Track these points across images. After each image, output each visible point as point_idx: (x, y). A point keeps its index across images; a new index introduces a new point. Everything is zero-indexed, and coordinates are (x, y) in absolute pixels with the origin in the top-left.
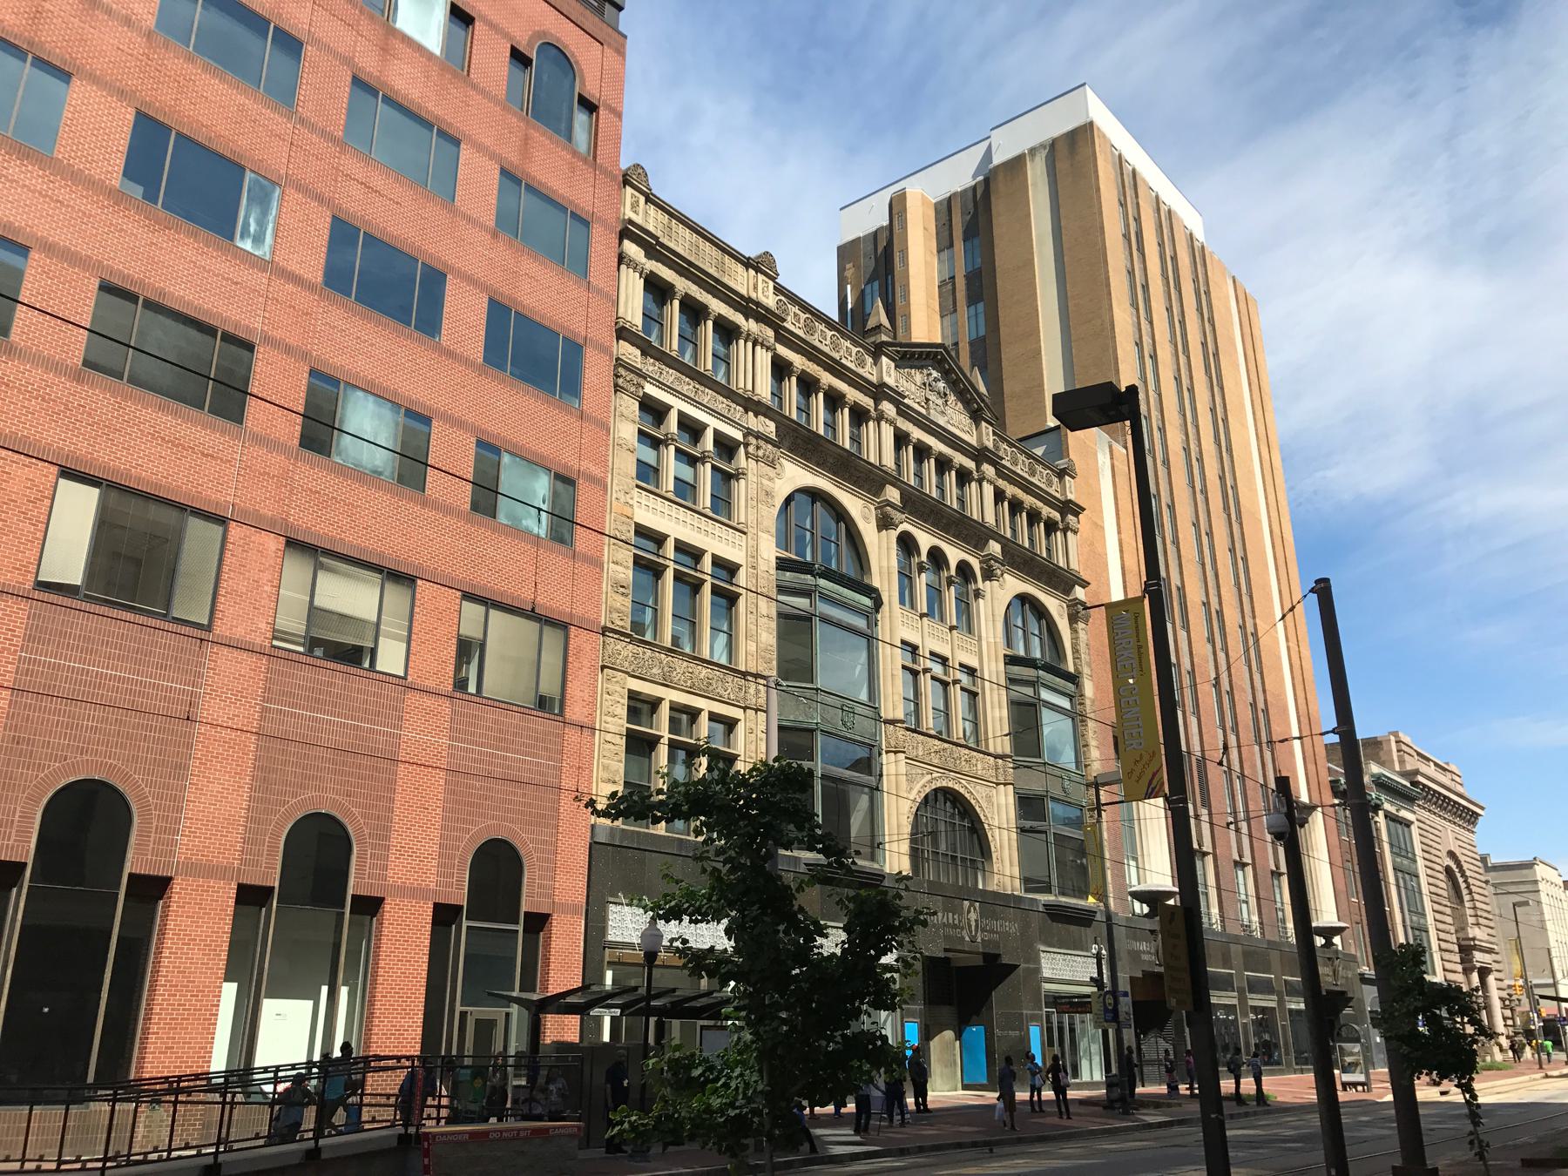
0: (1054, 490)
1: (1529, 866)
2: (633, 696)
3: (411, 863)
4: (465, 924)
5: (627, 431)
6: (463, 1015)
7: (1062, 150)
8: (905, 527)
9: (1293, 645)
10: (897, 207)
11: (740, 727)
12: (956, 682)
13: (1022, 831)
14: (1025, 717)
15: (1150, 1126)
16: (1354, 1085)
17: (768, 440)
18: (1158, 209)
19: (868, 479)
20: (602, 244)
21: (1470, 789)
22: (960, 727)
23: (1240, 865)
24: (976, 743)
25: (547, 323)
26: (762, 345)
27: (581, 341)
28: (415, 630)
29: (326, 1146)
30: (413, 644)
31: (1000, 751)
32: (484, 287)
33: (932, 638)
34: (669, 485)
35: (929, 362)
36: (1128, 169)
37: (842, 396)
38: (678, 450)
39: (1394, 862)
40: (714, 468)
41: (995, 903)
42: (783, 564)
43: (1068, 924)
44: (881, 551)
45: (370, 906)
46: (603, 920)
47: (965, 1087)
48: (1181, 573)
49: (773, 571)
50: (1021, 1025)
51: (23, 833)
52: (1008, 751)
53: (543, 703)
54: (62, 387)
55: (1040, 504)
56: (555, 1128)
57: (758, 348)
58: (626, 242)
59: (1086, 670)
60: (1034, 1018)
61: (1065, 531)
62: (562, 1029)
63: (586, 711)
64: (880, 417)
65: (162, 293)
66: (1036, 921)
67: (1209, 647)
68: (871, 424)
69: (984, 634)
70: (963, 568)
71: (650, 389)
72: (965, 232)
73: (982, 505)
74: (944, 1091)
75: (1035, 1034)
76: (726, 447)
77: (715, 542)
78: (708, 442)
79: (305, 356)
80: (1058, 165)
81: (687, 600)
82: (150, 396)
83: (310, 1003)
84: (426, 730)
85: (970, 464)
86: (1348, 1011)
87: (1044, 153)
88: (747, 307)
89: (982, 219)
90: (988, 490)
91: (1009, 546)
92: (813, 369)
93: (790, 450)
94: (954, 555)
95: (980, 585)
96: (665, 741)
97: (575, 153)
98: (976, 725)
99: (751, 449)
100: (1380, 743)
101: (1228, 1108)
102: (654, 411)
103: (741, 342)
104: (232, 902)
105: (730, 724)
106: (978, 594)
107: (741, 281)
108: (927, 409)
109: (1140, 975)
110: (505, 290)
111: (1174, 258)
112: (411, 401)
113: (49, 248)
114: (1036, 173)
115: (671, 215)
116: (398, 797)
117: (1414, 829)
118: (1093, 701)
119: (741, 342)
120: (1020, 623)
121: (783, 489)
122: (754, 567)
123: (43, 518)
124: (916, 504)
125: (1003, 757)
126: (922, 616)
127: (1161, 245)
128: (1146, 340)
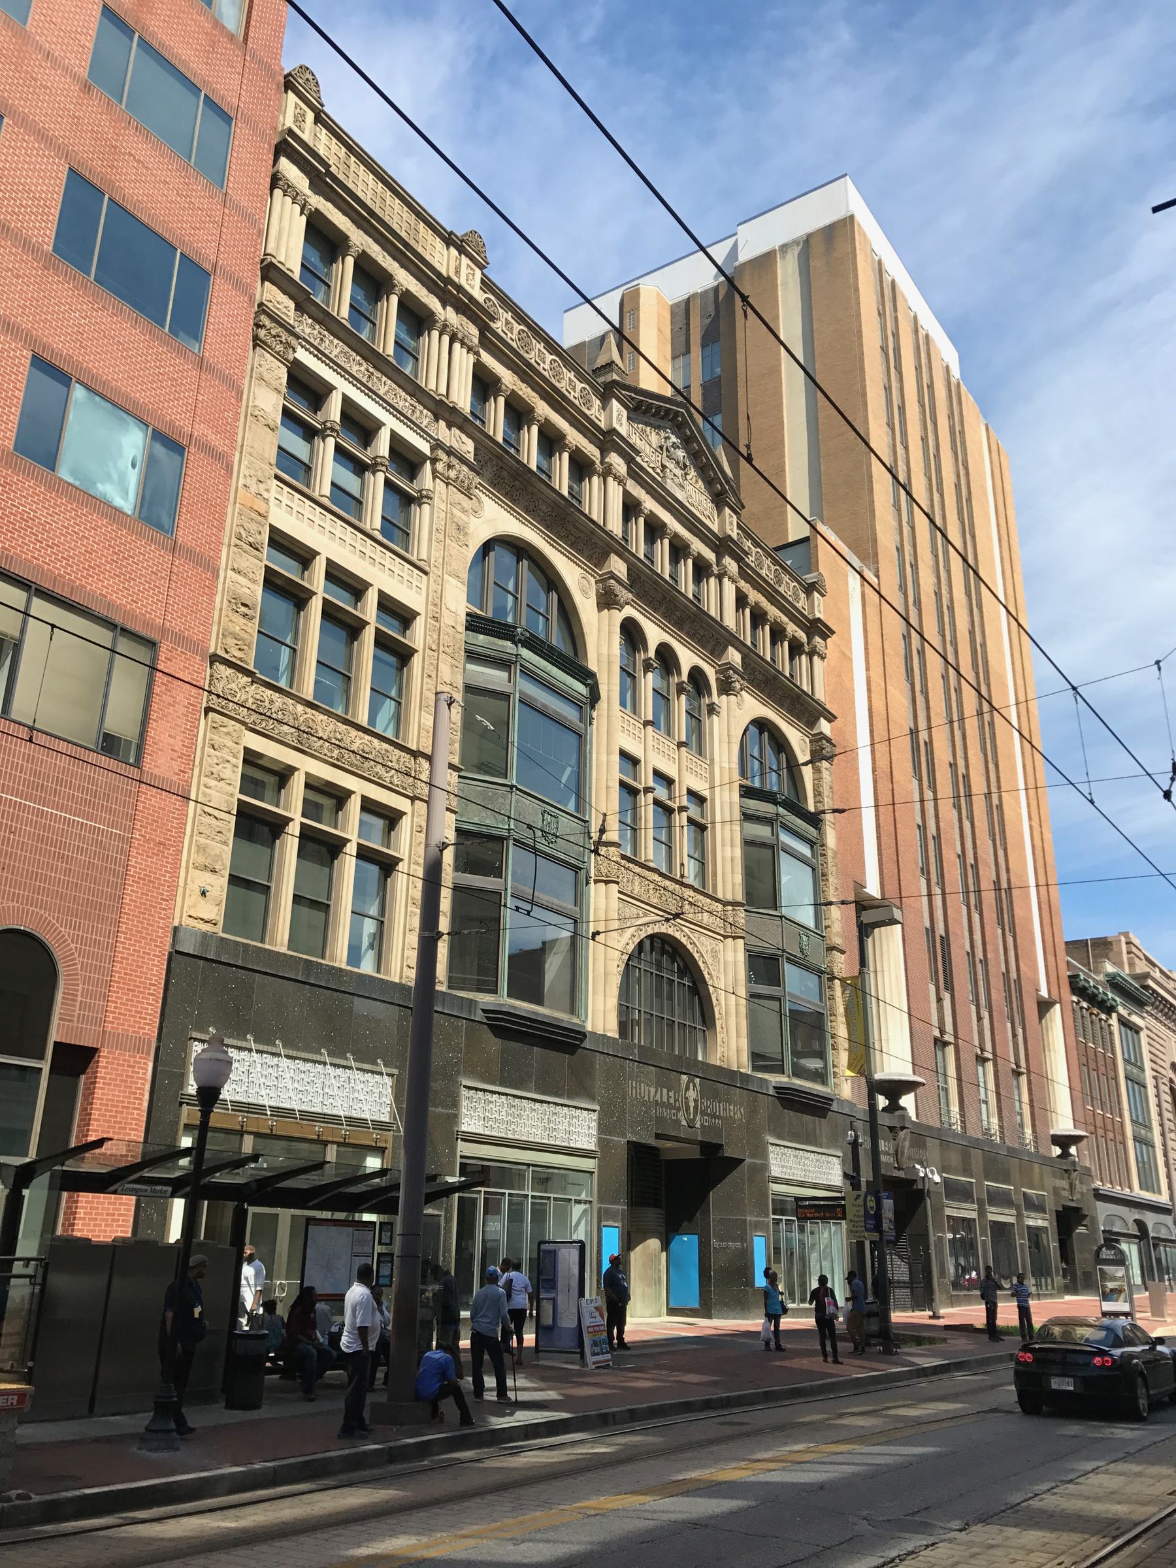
0: (802, 603)
2: (251, 758)
7: (818, 247)
8: (629, 611)
9: (1035, 824)
10: (629, 305)
11: (405, 824)
13: (752, 996)
15: (923, 1372)
17: (463, 460)
18: (916, 331)
20: (248, 157)
23: (982, 1060)
26: (463, 344)
29: (362, 1322)
31: (729, 898)
32: (63, 152)
34: (323, 488)
36: (887, 279)
37: (562, 436)
38: (339, 449)
39: (1125, 1069)
40: (388, 484)
41: (719, 1081)
42: (474, 624)
43: (805, 1110)
47: (672, 1312)
50: (742, 1233)
52: (740, 897)
53: (110, 744)
55: (785, 619)
57: (457, 346)
60: (757, 1226)
61: (811, 655)
62: (103, 1219)
63: (176, 766)
64: (607, 472)
66: (766, 1106)
67: (955, 813)
68: (595, 479)
69: (717, 757)
70: (696, 675)
71: (303, 356)
72: (704, 338)
73: (721, 601)
74: (647, 1319)
75: (759, 1246)
76: (406, 460)
77: (383, 574)
80: (813, 263)
81: (341, 648)
85: (710, 556)
86: (1081, 1230)
87: (797, 250)
91: (749, 654)
92: (526, 392)
94: (687, 658)
95: (715, 698)
96: (294, 829)
97: (217, 24)
98: (702, 864)
99: (440, 466)
100: (1110, 943)
102: (306, 387)
103: (435, 334)
105: (392, 818)
106: (712, 709)
107: (443, 259)
108: (664, 477)
110: (96, 167)
111: (931, 387)
114: (787, 272)
115: (349, 148)
117: (1143, 1034)
118: (835, 853)
119: (435, 334)
120: (756, 754)
121: (481, 532)
125: (734, 904)
126: (646, 723)
127: (918, 368)
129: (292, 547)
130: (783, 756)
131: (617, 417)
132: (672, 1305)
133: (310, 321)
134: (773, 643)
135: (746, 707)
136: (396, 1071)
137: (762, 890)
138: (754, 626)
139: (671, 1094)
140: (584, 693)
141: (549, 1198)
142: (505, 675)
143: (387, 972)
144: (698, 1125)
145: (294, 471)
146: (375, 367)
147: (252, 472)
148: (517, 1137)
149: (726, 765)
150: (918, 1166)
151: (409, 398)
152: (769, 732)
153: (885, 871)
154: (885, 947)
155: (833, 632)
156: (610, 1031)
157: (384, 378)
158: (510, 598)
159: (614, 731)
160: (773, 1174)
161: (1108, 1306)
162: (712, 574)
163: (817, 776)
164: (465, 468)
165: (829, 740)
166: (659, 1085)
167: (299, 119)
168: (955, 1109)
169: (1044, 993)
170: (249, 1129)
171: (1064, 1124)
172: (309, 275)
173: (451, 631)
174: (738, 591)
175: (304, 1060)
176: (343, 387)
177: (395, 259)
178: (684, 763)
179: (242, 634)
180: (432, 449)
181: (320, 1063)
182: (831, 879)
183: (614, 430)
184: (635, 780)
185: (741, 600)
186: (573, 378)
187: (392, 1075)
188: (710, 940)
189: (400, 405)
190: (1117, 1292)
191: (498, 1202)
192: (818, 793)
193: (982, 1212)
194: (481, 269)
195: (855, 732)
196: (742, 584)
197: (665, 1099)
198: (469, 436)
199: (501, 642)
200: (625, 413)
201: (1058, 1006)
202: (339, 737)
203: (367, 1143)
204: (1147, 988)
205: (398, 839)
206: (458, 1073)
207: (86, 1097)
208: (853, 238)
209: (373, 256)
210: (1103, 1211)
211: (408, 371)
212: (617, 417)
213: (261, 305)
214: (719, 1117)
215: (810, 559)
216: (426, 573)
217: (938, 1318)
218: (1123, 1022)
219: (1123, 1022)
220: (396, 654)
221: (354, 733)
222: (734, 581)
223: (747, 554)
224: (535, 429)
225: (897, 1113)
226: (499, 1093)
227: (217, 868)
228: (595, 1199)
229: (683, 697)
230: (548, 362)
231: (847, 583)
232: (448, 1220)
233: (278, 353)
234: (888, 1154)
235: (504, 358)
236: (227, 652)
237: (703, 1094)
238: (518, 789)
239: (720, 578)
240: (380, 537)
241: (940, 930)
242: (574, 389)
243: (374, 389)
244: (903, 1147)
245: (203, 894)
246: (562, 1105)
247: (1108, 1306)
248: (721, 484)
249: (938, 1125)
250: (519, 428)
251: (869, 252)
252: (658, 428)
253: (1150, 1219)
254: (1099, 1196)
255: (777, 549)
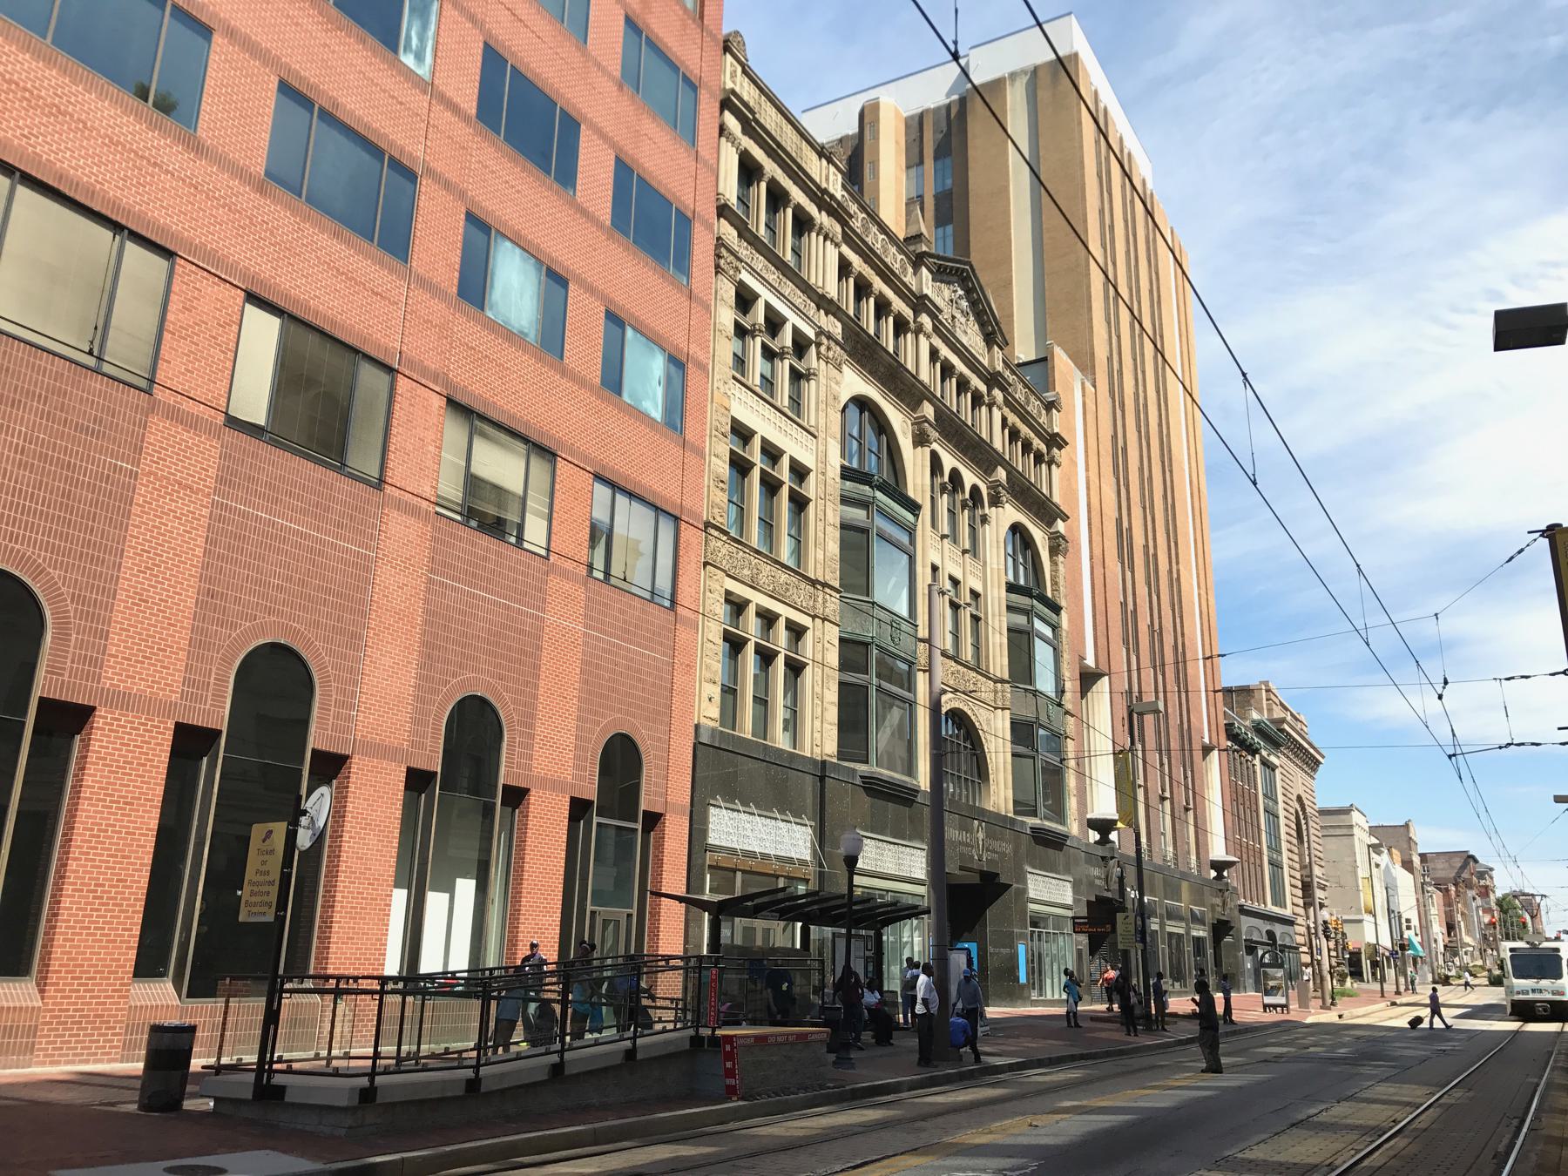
0: (1043, 419)
1: (1346, 811)
2: (729, 598)
3: (550, 758)
4: (596, 820)
5: (727, 316)
6: (593, 913)
7: (1044, 78)
9: (1203, 592)
10: (868, 117)
11: (809, 634)
14: (1020, 641)
16: (1275, 1006)
19: (906, 390)
21: (1315, 735)
22: (968, 653)
24: (978, 668)
25: (663, 191)
27: (690, 215)
28: (556, 508)
30: (554, 523)
32: (613, 145)
37: (889, 304)
41: (996, 823)
42: (847, 474)
44: (915, 463)
45: (516, 796)
46: (705, 820)
49: (838, 479)
51: (219, 696)
52: (1006, 677)
54: (247, 197)
56: (812, 1033)
58: (727, 113)
60: (1023, 936)
64: (919, 330)
65: (336, 105)
66: (1025, 840)
73: (991, 426)
75: (1021, 949)
76: (801, 346)
77: (794, 446)
78: (786, 338)
79: (462, 195)
80: (1040, 93)
82: (327, 221)
83: (446, 896)
84: (565, 615)
86: (1228, 939)
87: (1025, 79)
88: (821, 199)
89: (955, 141)
90: (997, 414)
94: (969, 478)
99: (823, 349)
101: (1222, 1028)
102: (745, 300)
104: (402, 786)
110: (629, 148)
112: (552, 259)
113: (231, 33)
116: (542, 684)
117: (1277, 772)
119: (814, 235)
122: (824, 474)
123: (232, 345)
125: (1003, 681)
130: (1029, 553)
134: (878, 317)
135: (1010, 513)
137: (1022, 668)
138: (858, 299)
143: (802, 749)
152: (870, 411)
161: (1268, 1000)
169: (1206, 740)
171: (1218, 851)
178: (968, 568)
180: (817, 335)
185: (844, 268)
187: (1548, 940)
190: (1277, 988)
192: (1055, 583)
193: (1162, 925)
196: (845, 249)
201: (1216, 752)
204: (1282, 731)
205: (805, 647)
207: (656, 848)
210: (1246, 923)
213: (719, 238)
218: (1265, 763)
219: (1265, 763)
220: (799, 503)
222: (837, 245)
223: (851, 217)
237: (989, 835)
240: (758, 390)
247: (1268, 1000)
252: (948, 283)
253: (1278, 929)
254: (1243, 910)
255: (1019, 365)
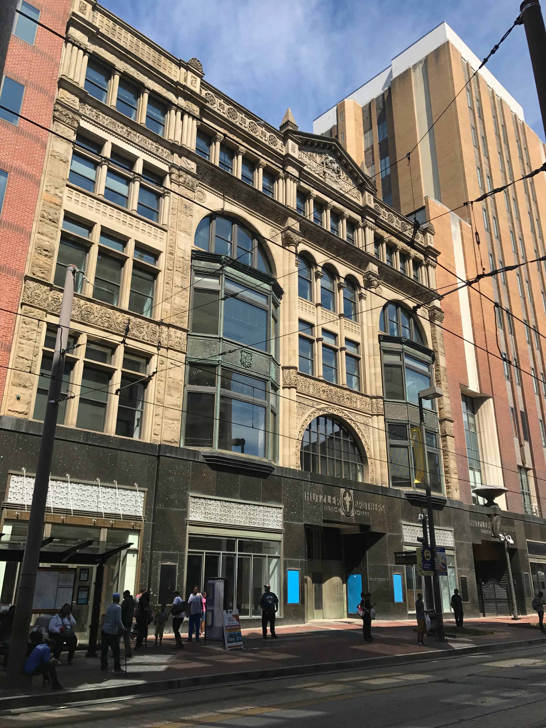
7: (431, 61)
8: (302, 247)
12: (342, 349)
18: (494, 98)
26: (190, 115)
27: (23, 83)
31: (374, 394)
33: (320, 319)
35: (326, 151)
47: (349, 616)
48: (509, 301)
50: (386, 573)
52: (380, 394)
57: (186, 117)
59: (440, 350)
61: (427, 266)
64: (288, 175)
66: (399, 505)
67: (529, 346)
68: (280, 181)
71: (84, 124)
73: (365, 239)
87: (421, 66)
93: (211, 185)
94: (343, 270)
99: (174, 176)
103: (173, 112)
107: (177, 74)
109: (480, 543)
111: (504, 126)
114: (417, 79)
122: (172, 254)
124: (311, 232)
125: (377, 397)
126: (317, 305)
128: (485, 167)
129: (81, 221)
131: (292, 148)
132: (349, 612)
133: (90, 108)
136: (146, 489)
139: (334, 499)
140: (269, 289)
141: (251, 555)
142: (217, 281)
144: (353, 515)
145: (82, 185)
146: (132, 129)
147: (51, 184)
148: (227, 523)
149: (370, 325)
150: (500, 535)
151: (154, 144)
153: (482, 378)
154: (484, 419)
155: (439, 253)
156: (292, 466)
157: (138, 134)
158: (395, 324)
159: (293, 310)
160: (405, 540)
162: (423, 265)
163: (433, 329)
164: (189, 177)
165: (439, 310)
166: (326, 494)
167: (83, 9)
168: (535, 504)
170: (48, 521)
172: (90, 84)
173: (181, 259)
174: (376, 234)
175: (85, 484)
176: (111, 140)
177: (145, 75)
178: (343, 324)
179: (44, 265)
181: (95, 485)
182: (443, 383)
183: (367, 206)
184: (312, 335)
186: (264, 130)
187: (144, 492)
188: (363, 417)
189: (149, 147)
191: (248, 560)
192: (434, 338)
194: (200, 77)
195: (459, 305)
197: (329, 501)
198: (192, 160)
199: (214, 264)
200: (297, 146)
202: (108, 316)
203: (127, 527)
206: (187, 489)
208: (449, 53)
209: (131, 74)
211: (230, 172)
212: (292, 148)
214: (367, 511)
215: (426, 216)
216: (166, 231)
217: (517, 619)
221: (118, 313)
224: (312, 201)
225: (492, 507)
226: (215, 500)
227: (27, 385)
228: (282, 556)
229: (342, 291)
230: (387, 216)
231: (451, 228)
232: (181, 568)
233: (68, 124)
234: (487, 529)
235: (218, 122)
236: (34, 275)
237: (356, 498)
238: (223, 339)
239: (364, 228)
240: (135, 213)
241: (521, 407)
242: (265, 136)
243: (132, 140)
244: (496, 525)
245: (18, 398)
246: (259, 505)
248: (362, 180)
249: (523, 513)
250: (321, 212)
251: (460, 58)
252: (320, 154)
255: (408, 216)
